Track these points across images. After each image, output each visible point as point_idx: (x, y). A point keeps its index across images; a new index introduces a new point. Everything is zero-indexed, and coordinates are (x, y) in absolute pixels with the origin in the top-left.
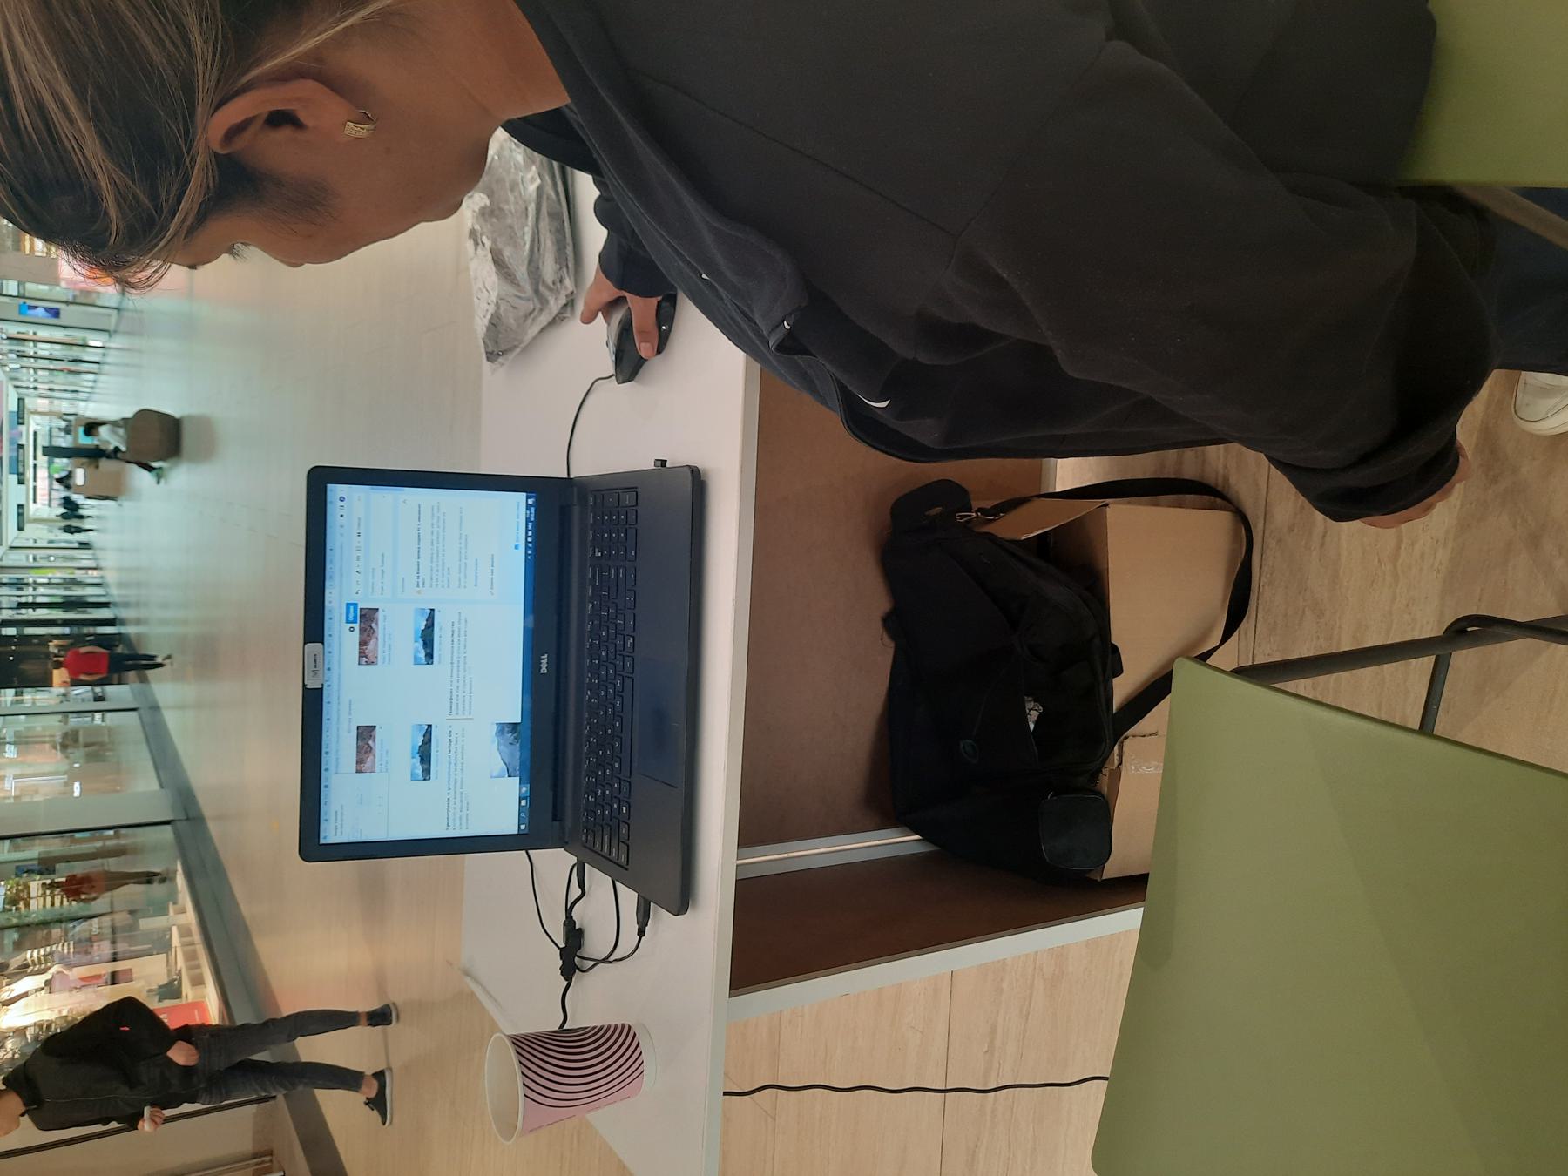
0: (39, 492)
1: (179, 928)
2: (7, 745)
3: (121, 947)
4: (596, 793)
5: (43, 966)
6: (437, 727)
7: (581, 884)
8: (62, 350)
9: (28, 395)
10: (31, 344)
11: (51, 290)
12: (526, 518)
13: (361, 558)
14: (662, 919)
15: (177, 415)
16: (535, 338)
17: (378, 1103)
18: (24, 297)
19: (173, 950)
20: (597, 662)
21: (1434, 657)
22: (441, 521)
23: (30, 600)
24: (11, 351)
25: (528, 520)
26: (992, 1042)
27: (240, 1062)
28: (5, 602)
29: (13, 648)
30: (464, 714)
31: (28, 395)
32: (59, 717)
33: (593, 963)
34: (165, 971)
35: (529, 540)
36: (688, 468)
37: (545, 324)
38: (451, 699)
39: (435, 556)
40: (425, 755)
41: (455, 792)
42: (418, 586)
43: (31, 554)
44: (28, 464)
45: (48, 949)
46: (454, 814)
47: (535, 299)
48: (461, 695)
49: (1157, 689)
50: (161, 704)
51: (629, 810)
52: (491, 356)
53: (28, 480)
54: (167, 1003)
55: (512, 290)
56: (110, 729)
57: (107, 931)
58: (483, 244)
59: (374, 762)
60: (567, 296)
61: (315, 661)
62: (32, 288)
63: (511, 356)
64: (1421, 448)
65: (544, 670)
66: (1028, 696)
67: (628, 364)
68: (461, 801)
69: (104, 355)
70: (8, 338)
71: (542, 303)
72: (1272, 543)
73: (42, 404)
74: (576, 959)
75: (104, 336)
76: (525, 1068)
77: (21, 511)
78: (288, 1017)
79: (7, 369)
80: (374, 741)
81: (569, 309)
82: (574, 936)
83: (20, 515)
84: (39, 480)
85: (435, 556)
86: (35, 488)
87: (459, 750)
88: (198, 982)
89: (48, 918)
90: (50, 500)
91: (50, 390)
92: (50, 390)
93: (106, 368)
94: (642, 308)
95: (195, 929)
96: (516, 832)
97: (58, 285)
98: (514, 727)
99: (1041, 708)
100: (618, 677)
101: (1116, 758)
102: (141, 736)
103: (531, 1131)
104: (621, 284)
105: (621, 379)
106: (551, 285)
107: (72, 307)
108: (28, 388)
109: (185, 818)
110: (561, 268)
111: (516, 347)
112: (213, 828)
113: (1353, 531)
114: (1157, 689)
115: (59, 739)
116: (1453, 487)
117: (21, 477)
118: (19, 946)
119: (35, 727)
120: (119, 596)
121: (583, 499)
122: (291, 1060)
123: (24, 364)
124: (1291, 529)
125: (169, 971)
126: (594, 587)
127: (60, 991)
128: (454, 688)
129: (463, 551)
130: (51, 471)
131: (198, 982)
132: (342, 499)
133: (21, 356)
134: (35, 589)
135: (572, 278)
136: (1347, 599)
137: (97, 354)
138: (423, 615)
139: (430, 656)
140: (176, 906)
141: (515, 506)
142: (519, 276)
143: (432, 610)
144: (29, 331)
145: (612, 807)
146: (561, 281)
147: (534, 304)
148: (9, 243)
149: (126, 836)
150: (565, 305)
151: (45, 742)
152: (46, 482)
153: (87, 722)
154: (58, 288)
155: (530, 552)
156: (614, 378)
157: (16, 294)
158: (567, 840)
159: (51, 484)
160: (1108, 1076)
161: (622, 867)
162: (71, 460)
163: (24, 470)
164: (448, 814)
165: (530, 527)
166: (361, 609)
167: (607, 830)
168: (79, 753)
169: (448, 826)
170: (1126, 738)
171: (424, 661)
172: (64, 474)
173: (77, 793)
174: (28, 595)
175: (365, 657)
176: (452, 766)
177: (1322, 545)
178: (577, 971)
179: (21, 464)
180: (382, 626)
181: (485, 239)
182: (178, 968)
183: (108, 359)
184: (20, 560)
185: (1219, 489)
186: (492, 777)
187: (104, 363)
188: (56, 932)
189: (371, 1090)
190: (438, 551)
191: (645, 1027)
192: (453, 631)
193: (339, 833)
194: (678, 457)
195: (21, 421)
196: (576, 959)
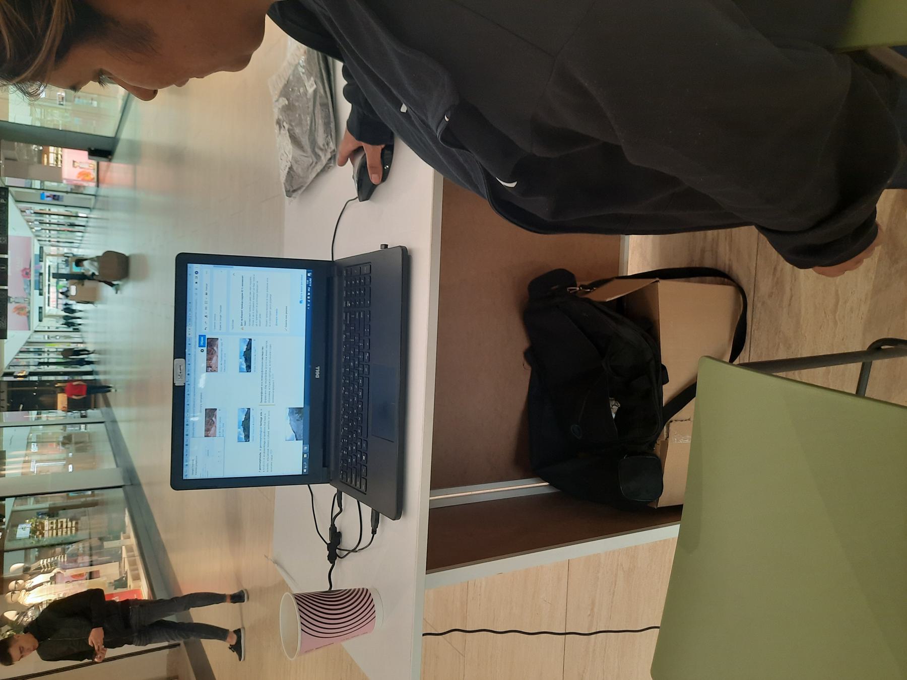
0: (51, 300)
1: (126, 547)
2: (33, 443)
3: (94, 558)
4: (348, 449)
5: (49, 569)
6: (253, 410)
7: (340, 505)
8: (65, 219)
9: (46, 245)
10: (47, 216)
11: (58, 185)
12: (307, 285)
13: (208, 308)
14: (386, 523)
15: (127, 254)
16: (313, 181)
17: (237, 648)
18: (42, 189)
19: (123, 559)
20: (348, 370)
21: (861, 364)
22: (256, 286)
23: (46, 360)
24: (36, 220)
25: (307, 286)
26: (592, 609)
27: (157, 621)
28: (32, 362)
29: (36, 388)
30: (269, 402)
31: (46, 245)
32: (61, 427)
33: (347, 552)
34: (118, 572)
35: (309, 298)
36: (399, 248)
37: (319, 171)
38: (262, 393)
39: (252, 307)
40: (246, 425)
41: (264, 450)
42: (242, 325)
43: (46, 334)
44: (45, 283)
45: (52, 559)
46: (264, 461)
47: (313, 156)
48: (268, 390)
49: (688, 393)
50: (118, 419)
51: (366, 458)
52: (289, 193)
53: (45, 293)
54: (119, 590)
55: (299, 152)
56: (89, 435)
57: (87, 549)
58: (284, 127)
59: (215, 430)
60: (331, 153)
62: (48, 184)
63: (300, 192)
64: (853, 217)
65: (317, 376)
66: (611, 397)
67: (366, 190)
68: (268, 455)
69: (87, 222)
70: (35, 213)
71: (317, 159)
72: (759, 305)
73: (53, 250)
74: (337, 550)
75: (87, 211)
76: (302, 613)
77: (40, 310)
78: (185, 596)
79: (34, 230)
80: (216, 418)
81: (332, 161)
82: (336, 536)
83: (40, 313)
84: (51, 293)
85: (252, 307)
86: (49, 297)
87: (267, 424)
88: (136, 578)
89: (53, 542)
90: (57, 304)
91: (58, 242)
92: (58, 242)
93: (88, 229)
94: (372, 152)
95: (135, 548)
96: (301, 474)
97: (62, 182)
98: (299, 410)
99: (619, 404)
100: (360, 377)
101: (665, 434)
102: (106, 437)
103: (306, 652)
104: (360, 137)
105: (361, 199)
106: (322, 146)
107: (69, 195)
108: (45, 241)
109: (130, 484)
110: (327, 137)
111: (302, 186)
112: (146, 489)
113: (808, 277)
114: (688, 393)
115: (61, 439)
116: (873, 249)
117: (41, 291)
118: (38, 558)
119: (47, 433)
120: (95, 358)
121: (340, 273)
122: (186, 622)
123: (43, 227)
124: (770, 296)
125: (120, 573)
126: (346, 325)
127: (61, 583)
128: (264, 386)
129: (269, 304)
130: (58, 288)
131: (136, 578)
132: (197, 272)
133: (41, 223)
134: (48, 354)
135: (334, 140)
136: (805, 336)
137: (83, 221)
138: (245, 342)
139: (249, 368)
140: (125, 535)
141: (300, 277)
142: (303, 143)
143: (250, 340)
144: (46, 208)
145: (356, 456)
146: (328, 144)
147: (312, 159)
148: (36, 159)
149: (98, 495)
150: (330, 159)
151: (54, 442)
152: (55, 295)
153: (76, 430)
154: (62, 185)
155: (309, 305)
156: (358, 199)
157: (39, 188)
158: (331, 478)
159: (57, 296)
160: (659, 626)
161: (363, 493)
162: (68, 282)
163: (43, 287)
164: (260, 463)
165: (309, 290)
166: (208, 339)
167: (354, 471)
168: (72, 447)
169: (260, 469)
170: (671, 422)
171: (245, 370)
172: (65, 290)
173: (70, 470)
174: (44, 358)
175: (210, 368)
176: (263, 433)
177: (790, 305)
178: (337, 558)
179: (41, 284)
180: (220, 348)
181: (285, 124)
182: (126, 570)
183: (90, 224)
184: (40, 338)
185: (727, 273)
186: (286, 440)
187: (88, 226)
188: (58, 549)
189: (233, 640)
190: (253, 304)
191: (377, 590)
192: (263, 352)
193: (194, 473)
194: (393, 242)
195: (41, 260)
196: (337, 550)
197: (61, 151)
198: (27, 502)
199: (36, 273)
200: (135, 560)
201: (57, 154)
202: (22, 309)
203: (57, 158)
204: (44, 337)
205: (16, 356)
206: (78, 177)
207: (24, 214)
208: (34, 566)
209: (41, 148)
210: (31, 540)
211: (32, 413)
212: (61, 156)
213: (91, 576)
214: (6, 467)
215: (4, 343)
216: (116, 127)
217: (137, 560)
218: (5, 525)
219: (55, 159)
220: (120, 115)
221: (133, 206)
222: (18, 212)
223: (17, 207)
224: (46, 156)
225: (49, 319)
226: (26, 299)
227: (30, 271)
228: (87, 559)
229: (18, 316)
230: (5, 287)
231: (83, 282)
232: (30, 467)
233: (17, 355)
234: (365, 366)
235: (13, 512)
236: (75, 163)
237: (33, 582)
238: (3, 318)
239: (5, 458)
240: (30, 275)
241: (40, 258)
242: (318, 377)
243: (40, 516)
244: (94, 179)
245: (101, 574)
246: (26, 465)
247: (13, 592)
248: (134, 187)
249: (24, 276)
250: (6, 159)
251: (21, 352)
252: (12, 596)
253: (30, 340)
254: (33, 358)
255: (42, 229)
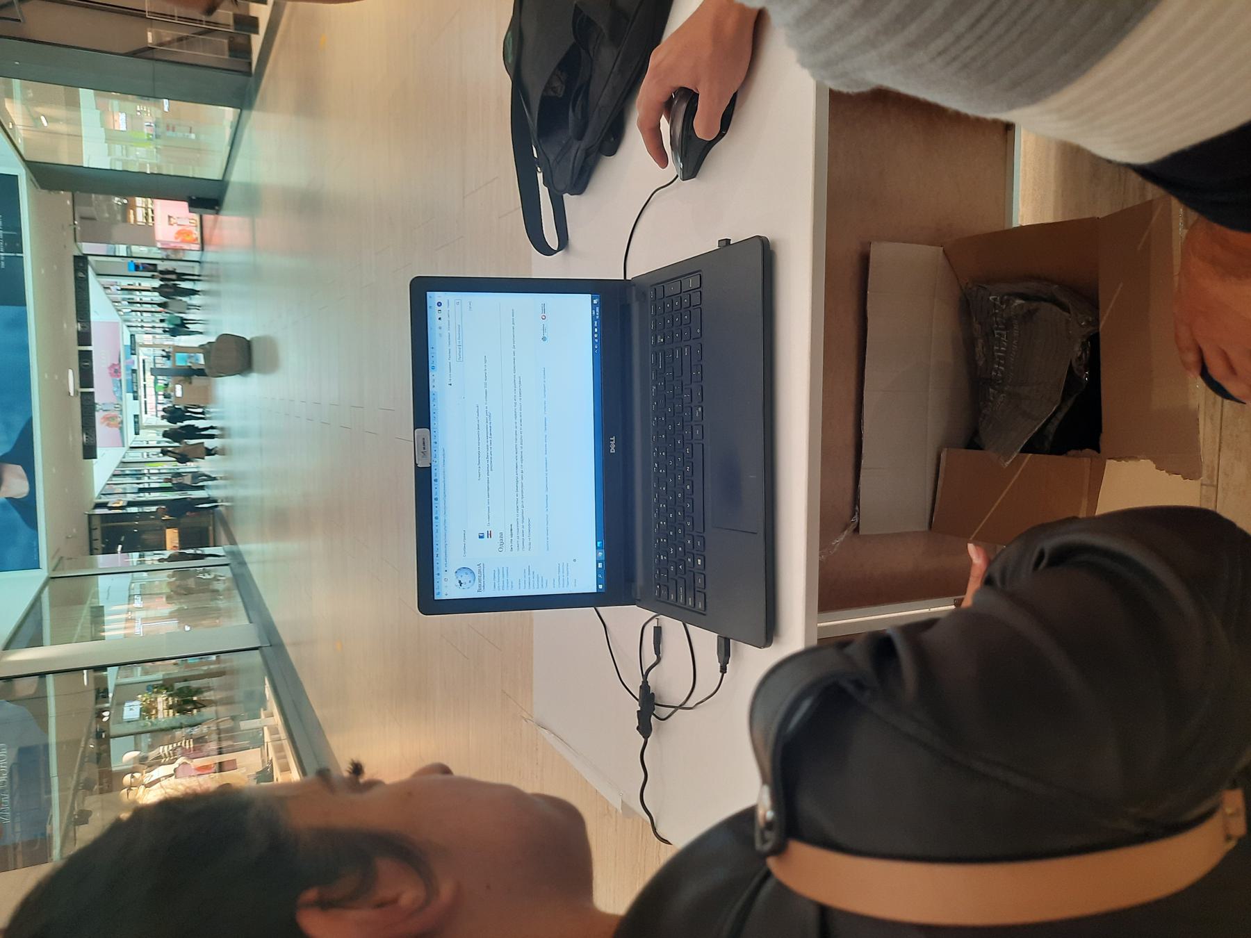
5: (167, 760)
10: (137, 293)
19: (266, 744)
24: (124, 299)
29: (137, 523)
34: (260, 761)
35: (596, 336)
61: (424, 443)
62: (138, 250)
65: (613, 451)
70: (122, 289)
73: (148, 339)
83: (136, 423)
86: (145, 402)
91: (153, 327)
92: (153, 327)
112: (291, 651)
118: (152, 747)
125: (263, 761)
131: (285, 769)
133: (131, 303)
144: (135, 283)
148: (119, 217)
155: (596, 347)
165: (596, 325)
167: (681, 582)
195: (133, 352)
197: (152, 204)
198: (132, 672)
199: (127, 370)
200: (282, 744)
201: (146, 209)
202: (114, 418)
203: (147, 214)
204: (143, 456)
205: (108, 481)
206: (176, 238)
207: (109, 291)
208: (153, 754)
209: (125, 201)
210: (142, 723)
211: (132, 555)
212: (152, 211)
213: (221, 767)
214: (106, 627)
215: (93, 464)
216: (223, 171)
217: (284, 745)
218: (108, 702)
219: (145, 215)
220: (229, 148)
221: (254, 275)
222: (101, 289)
223: (99, 281)
224: (132, 212)
225: (146, 431)
226: (117, 406)
227: (120, 368)
228: (213, 746)
229: (107, 427)
230: (91, 390)
231: (191, 379)
232: (134, 627)
233: (111, 477)
234: (694, 427)
235: (117, 686)
236: (172, 219)
237: (152, 776)
238: (91, 431)
239: (103, 615)
240: (120, 373)
241: (132, 349)
242: (614, 452)
243: (155, 690)
244: (197, 239)
245: (238, 765)
246: (128, 625)
247: (130, 788)
248: (253, 246)
249: (112, 375)
250: (82, 218)
251: (114, 475)
252: (128, 794)
253: (125, 460)
254: (130, 484)
255: (133, 311)
